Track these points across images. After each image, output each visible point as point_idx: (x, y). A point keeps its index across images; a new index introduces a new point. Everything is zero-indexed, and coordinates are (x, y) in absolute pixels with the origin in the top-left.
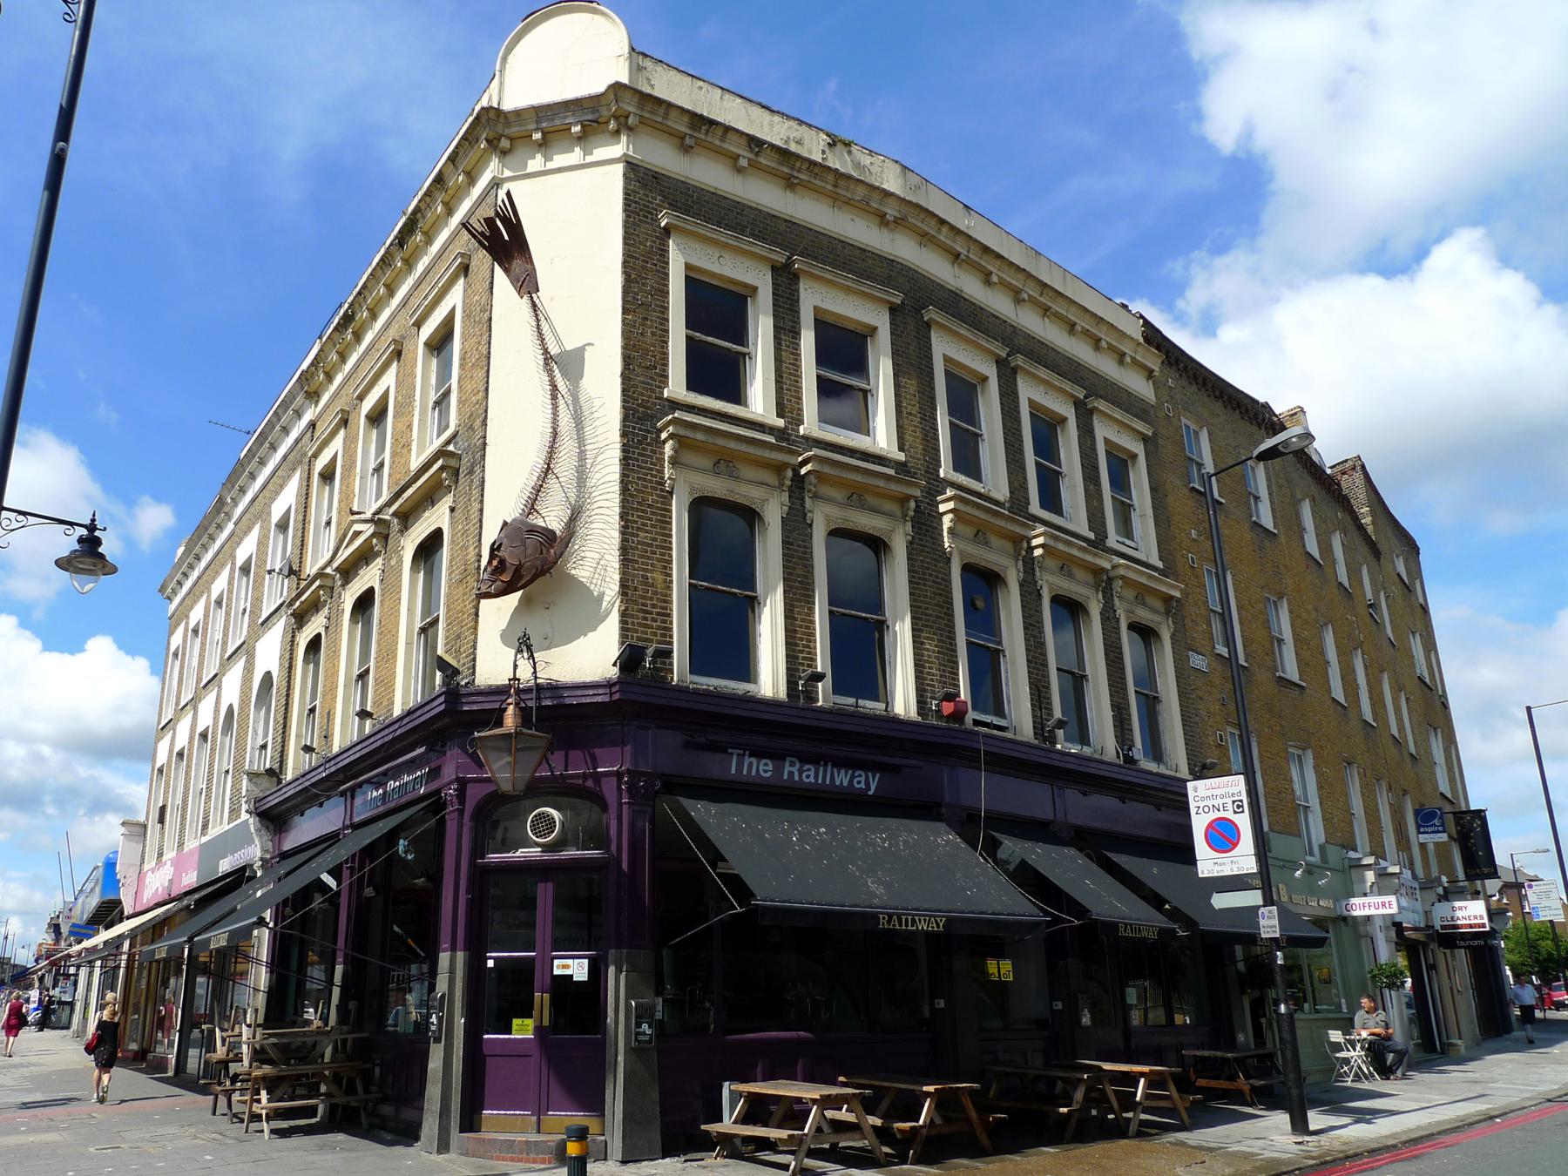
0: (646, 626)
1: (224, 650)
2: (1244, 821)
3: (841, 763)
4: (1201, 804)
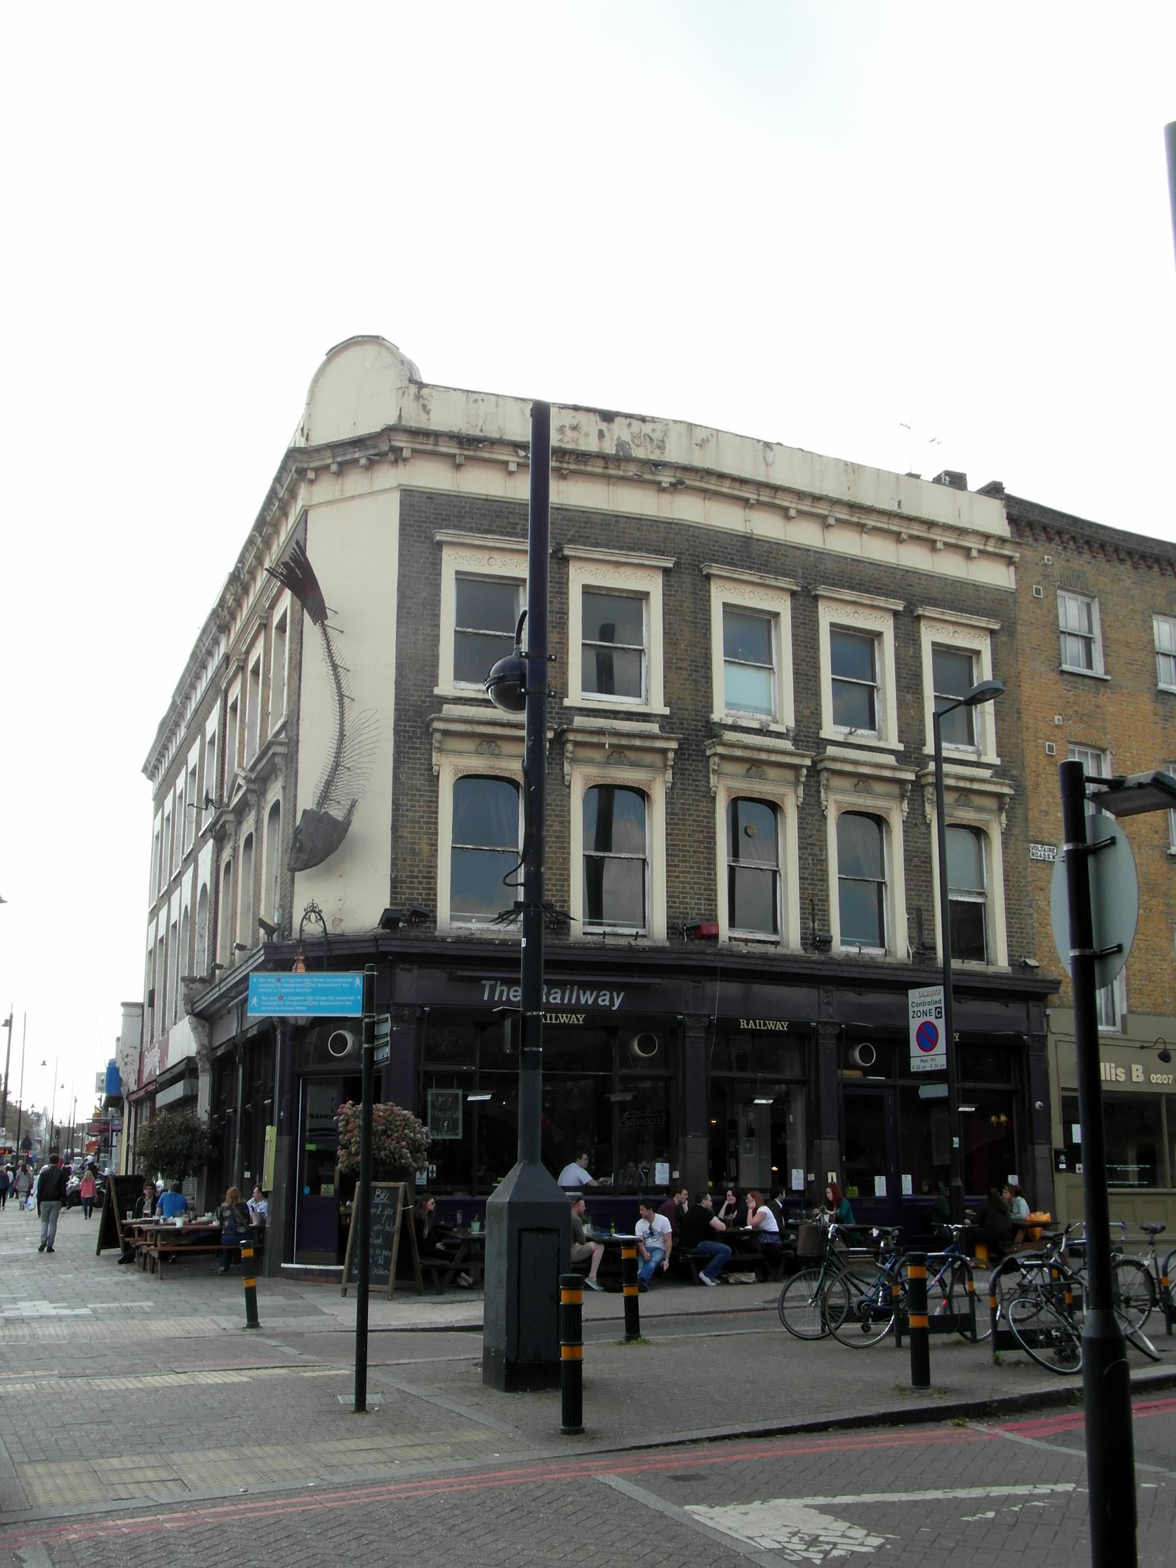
0: (413, 888)
1: (198, 828)
2: (940, 1025)
3: (586, 986)
4: (916, 1009)
